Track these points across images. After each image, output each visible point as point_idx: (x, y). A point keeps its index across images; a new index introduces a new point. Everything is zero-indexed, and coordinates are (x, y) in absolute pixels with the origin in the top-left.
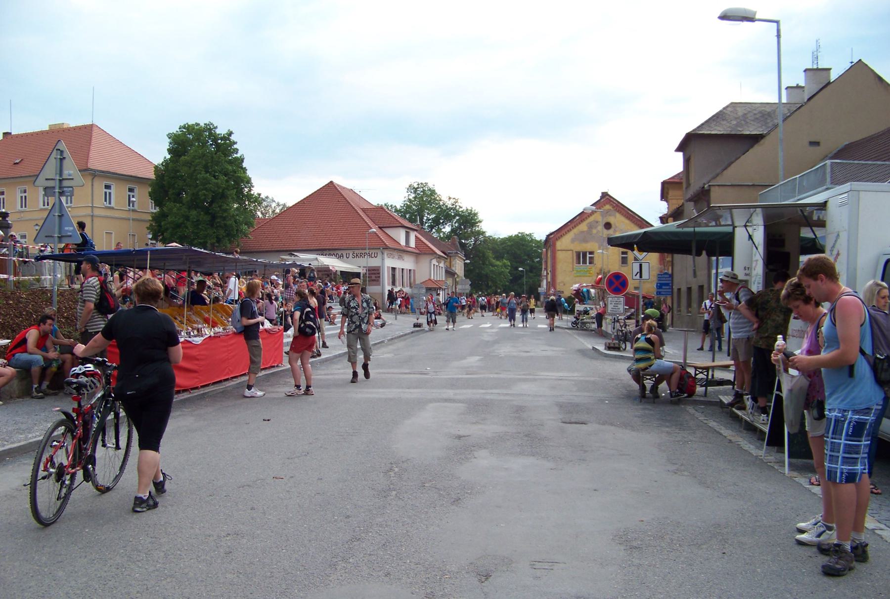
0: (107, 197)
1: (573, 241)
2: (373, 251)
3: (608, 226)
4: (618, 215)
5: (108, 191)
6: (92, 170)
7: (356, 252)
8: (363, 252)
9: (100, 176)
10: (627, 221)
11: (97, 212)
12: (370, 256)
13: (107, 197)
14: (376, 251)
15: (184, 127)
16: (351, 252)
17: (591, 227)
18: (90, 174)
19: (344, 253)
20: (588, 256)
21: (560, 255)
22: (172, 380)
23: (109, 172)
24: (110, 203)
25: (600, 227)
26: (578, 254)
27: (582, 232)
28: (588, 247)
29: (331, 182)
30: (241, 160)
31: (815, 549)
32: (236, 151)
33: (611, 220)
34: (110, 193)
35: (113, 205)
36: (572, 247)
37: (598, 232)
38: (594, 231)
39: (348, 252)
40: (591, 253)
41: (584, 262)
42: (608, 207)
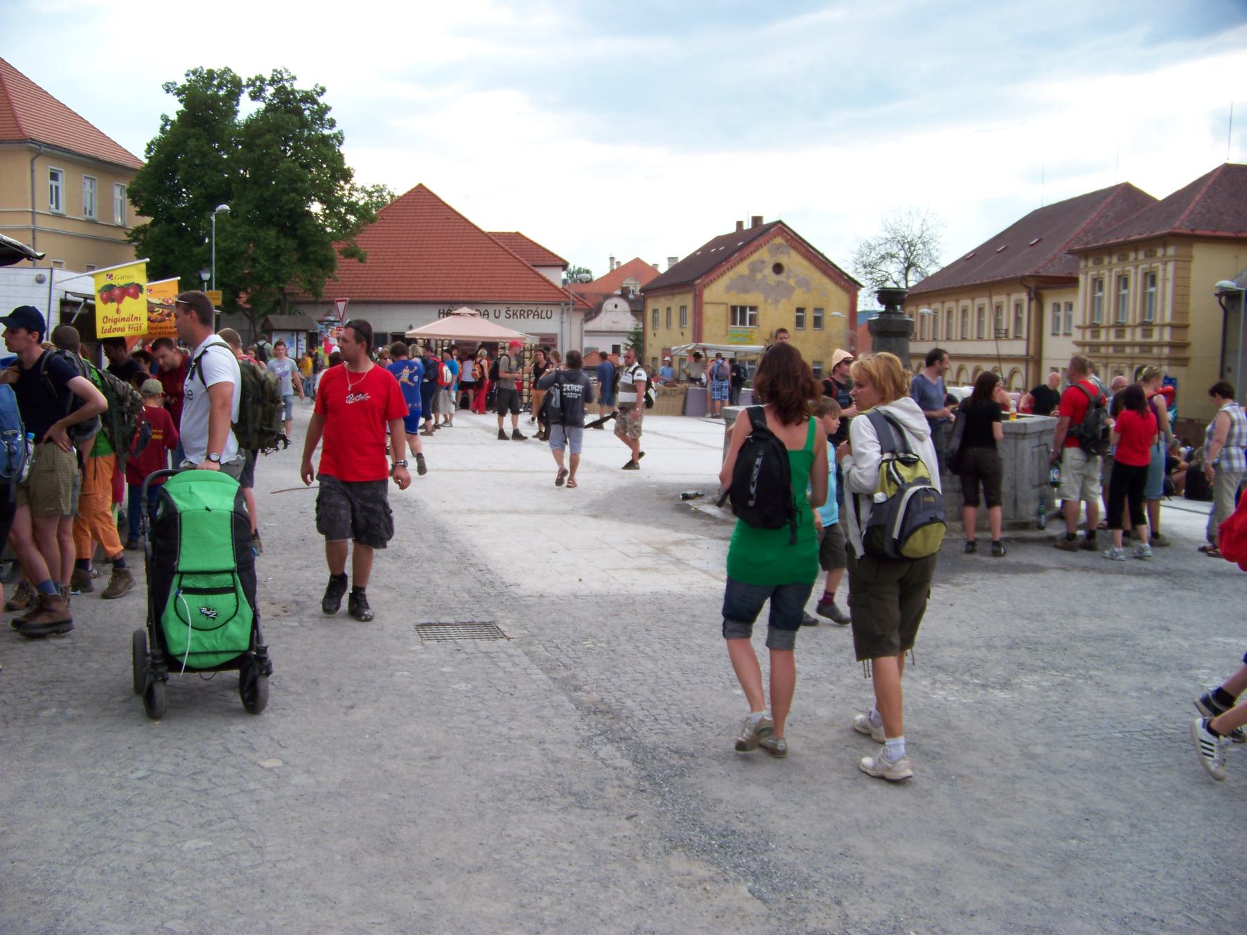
0: (55, 194)
1: (728, 289)
2: (545, 308)
3: (778, 268)
4: (793, 253)
5: (54, 183)
6: (33, 141)
7: (513, 308)
8: (526, 308)
9: (47, 155)
10: (806, 263)
11: (41, 223)
12: (540, 316)
13: (55, 194)
14: (549, 308)
15: (194, 73)
16: (503, 309)
17: (754, 269)
18: (31, 150)
19: (491, 309)
20: (748, 313)
21: (708, 311)
22: (885, 653)
23: (68, 151)
24: (57, 207)
25: (768, 270)
26: (734, 309)
27: (742, 277)
28: (748, 299)
29: (420, 185)
30: (339, 138)
31: (874, 737)
32: (332, 124)
33: (783, 260)
34: (57, 188)
35: (62, 210)
36: (725, 298)
37: (765, 277)
38: (759, 276)
39: (497, 307)
40: (752, 308)
41: (743, 322)
42: (779, 240)
